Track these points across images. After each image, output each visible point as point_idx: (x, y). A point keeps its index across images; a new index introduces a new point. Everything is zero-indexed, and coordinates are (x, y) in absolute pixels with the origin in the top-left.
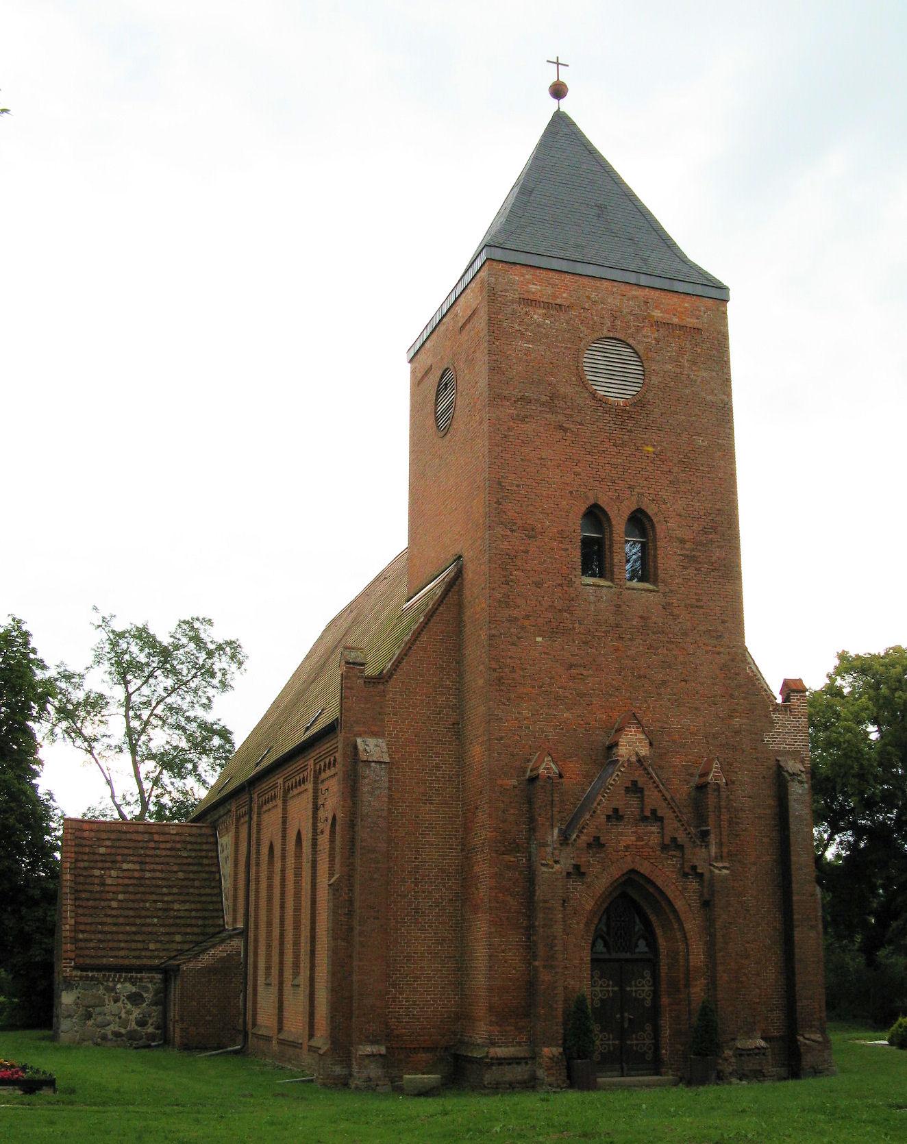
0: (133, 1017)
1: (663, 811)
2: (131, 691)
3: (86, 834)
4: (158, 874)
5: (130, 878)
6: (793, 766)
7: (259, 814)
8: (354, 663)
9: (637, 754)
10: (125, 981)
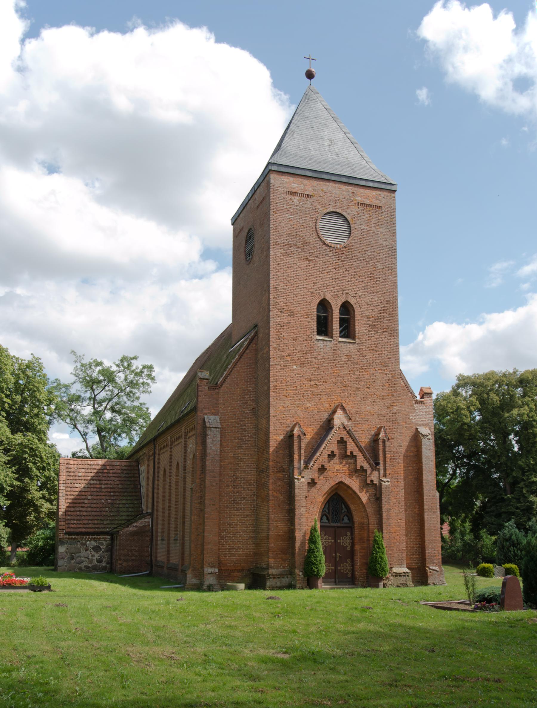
0: (95, 558)
1: (357, 452)
2: (96, 394)
3: (72, 466)
4: (109, 486)
5: (94, 488)
6: (424, 431)
7: (159, 455)
8: (203, 379)
9: (343, 424)
10: (91, 540)
